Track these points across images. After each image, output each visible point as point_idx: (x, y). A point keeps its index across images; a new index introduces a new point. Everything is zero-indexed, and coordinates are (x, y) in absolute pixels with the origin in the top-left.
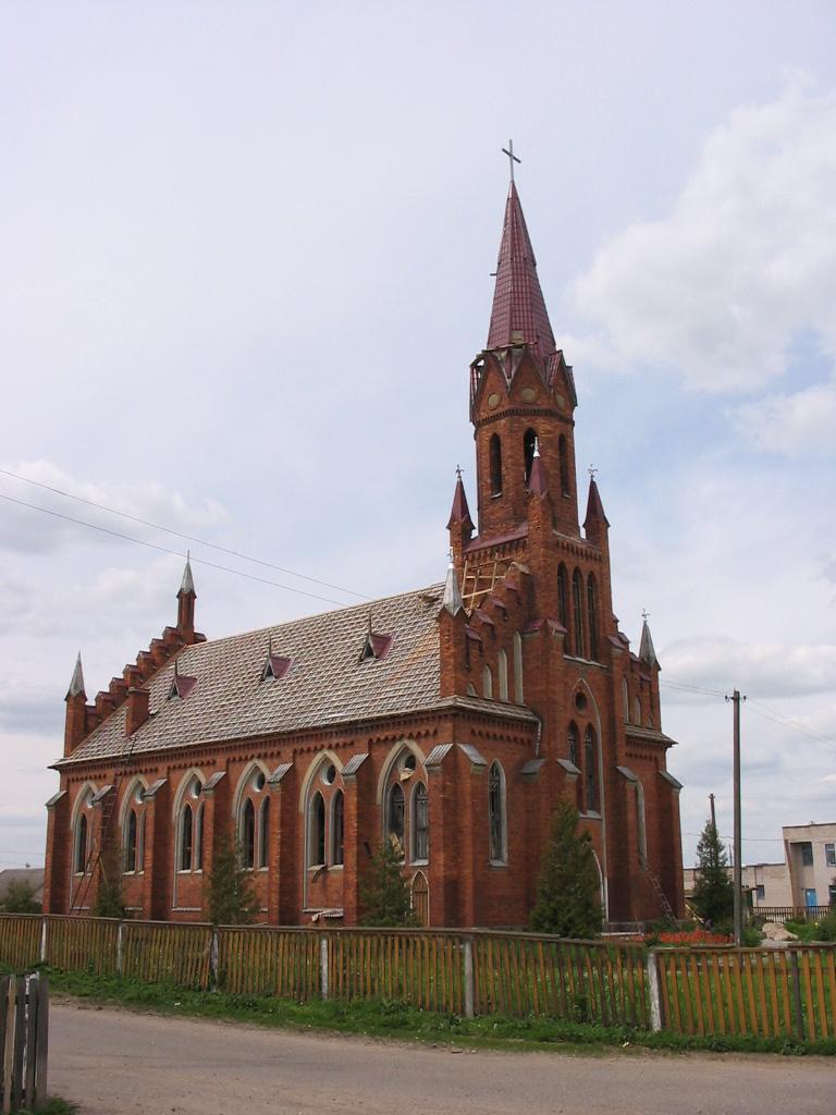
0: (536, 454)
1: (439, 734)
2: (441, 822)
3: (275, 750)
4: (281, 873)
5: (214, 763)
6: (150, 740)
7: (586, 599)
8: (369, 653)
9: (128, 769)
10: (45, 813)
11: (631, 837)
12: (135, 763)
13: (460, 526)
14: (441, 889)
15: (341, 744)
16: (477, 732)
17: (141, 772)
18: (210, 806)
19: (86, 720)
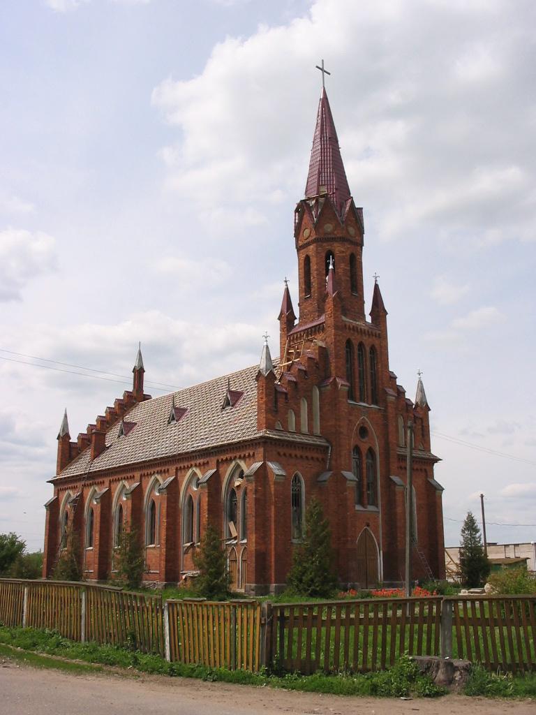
0: (331, 267)
1: (256, 456)
2: (254, 514)
3: (166, 468)
4: (166, 548)
5: (134, 476)
7: (368, 363)
8: (228, 404)
10: (44, 510)
11: (399, 524)
12: (93, 478)
13: (287, 318)
14: (254, 559)
16: (282, 453)
19: (70, 451)
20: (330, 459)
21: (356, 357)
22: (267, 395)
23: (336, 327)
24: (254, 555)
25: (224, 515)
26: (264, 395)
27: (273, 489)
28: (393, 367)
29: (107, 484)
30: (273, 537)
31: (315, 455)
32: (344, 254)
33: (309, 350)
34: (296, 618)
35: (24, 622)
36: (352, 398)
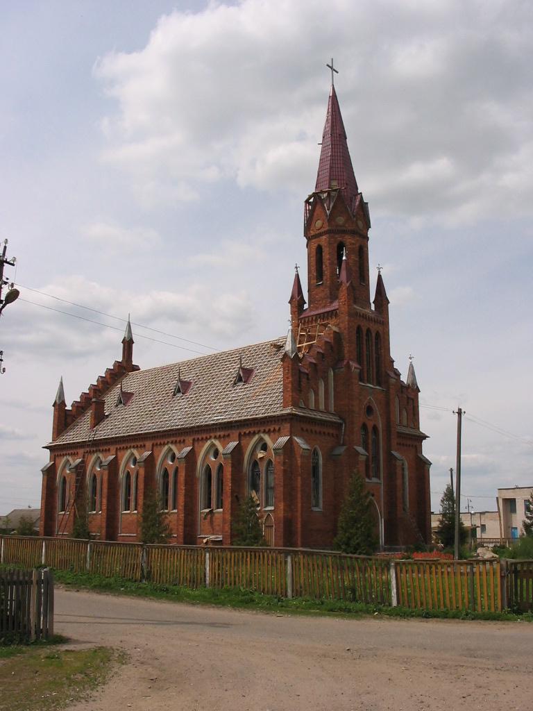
2: (282, 484)
3: (182, 439)
5: (144, 446)
6: (106, 431)
8: (240, 379)
9: (92, 449)
13: (297, 302)
15: (222, 436)
16: (305, 429)
17: (99, 451)
18: (142, 472)
19: (66, 419)
20: (344, 435)
21: (365, 342)
22: (292, 376)
23: (350, 315)
24: (282, 522)
25: (247, 484)
26: (290, 375)
27: (299, 462)
28: (393, 355)
29: (113, 451)
30: (299, 505)
31: (331, 431)
32: (354, 246)
33: (323, 335)
34: (525, 571)
35: (207, 582)
36: (361, 380)
